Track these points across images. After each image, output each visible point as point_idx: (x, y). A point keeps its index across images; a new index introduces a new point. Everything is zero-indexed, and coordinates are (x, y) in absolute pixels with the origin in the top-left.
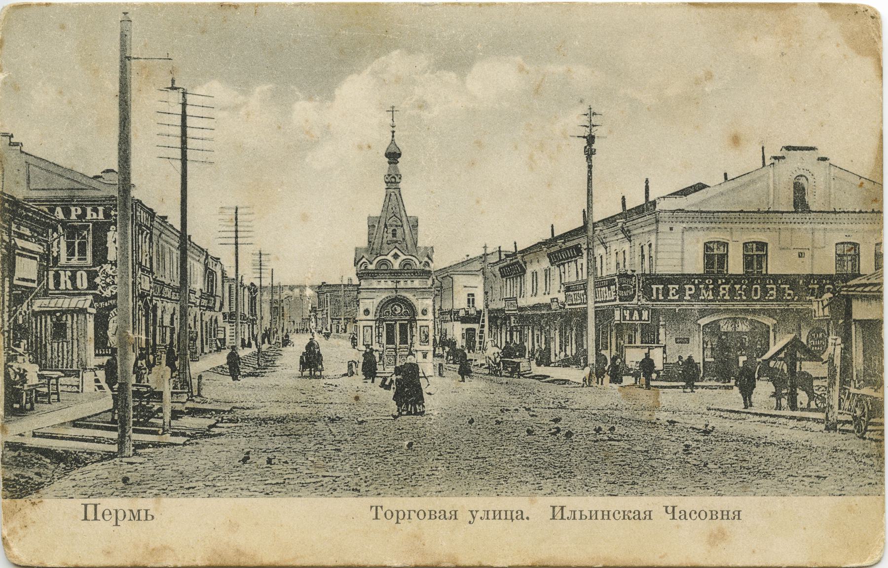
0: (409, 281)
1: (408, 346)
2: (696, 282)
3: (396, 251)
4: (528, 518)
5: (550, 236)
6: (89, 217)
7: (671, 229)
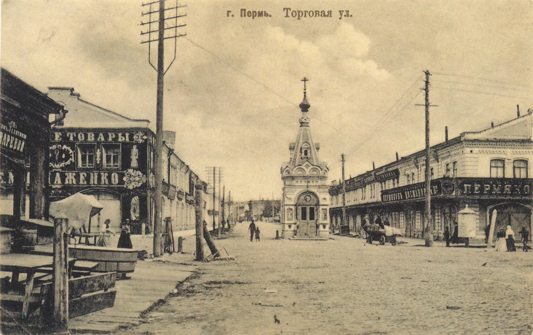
0: (315, 181)
1: (315, 221)
2: (491, 182)
3: (307, 163)
4: (233, 16)
5: (444, 140)
6: (120, 140)
7: (471, 151)
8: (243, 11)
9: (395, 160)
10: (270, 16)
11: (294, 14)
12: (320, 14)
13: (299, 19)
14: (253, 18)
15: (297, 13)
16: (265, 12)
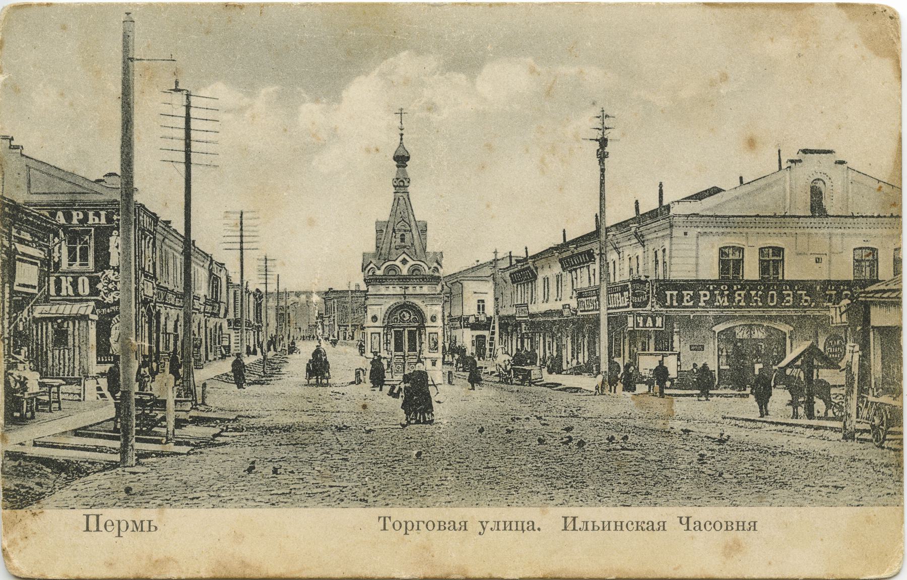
0: (418, 287)
1: (417, 353)
2: (711, 288)
3: (404, 256)
6: (90, 222)
7: (686, 234)
9: (561, 241)
11: (397, 526)
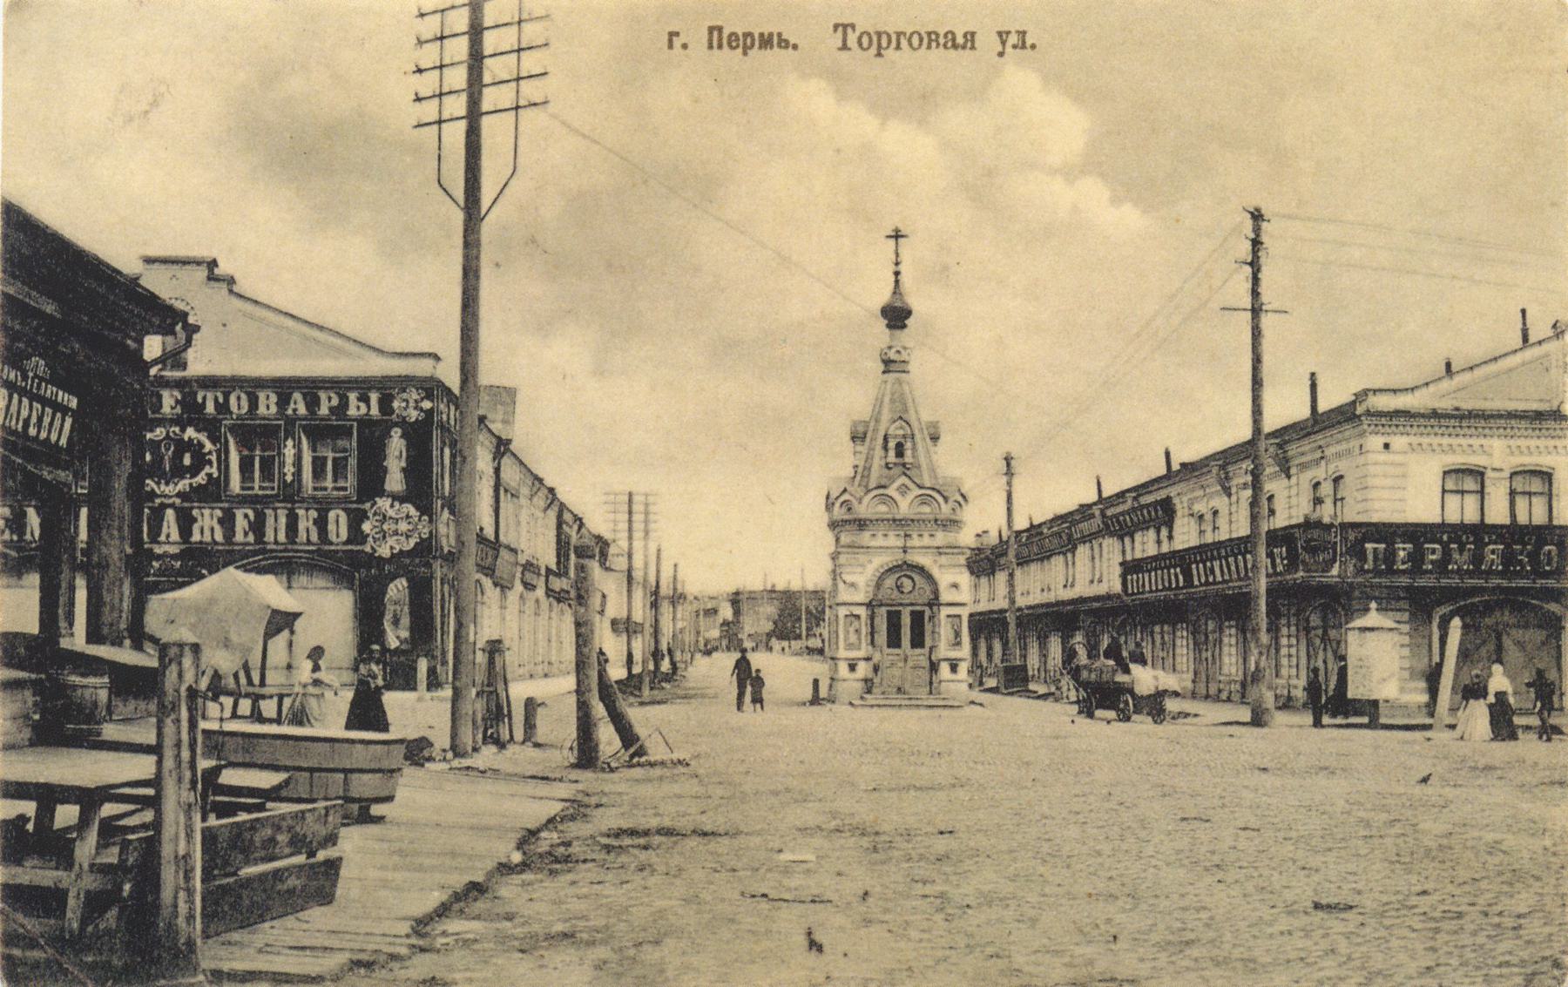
0: (926, 535)
1: (926, 651)
2: (1445, 538)
3: (904, 480)
4: (685, 46)
5: (1305, 413)
6: (352, 412)
7: (1387, 446)
8: (715, 34)
9: (1163, 471)
10: (795, 47)
11: (865, 40)
12: (942, 41)
13: (879, 55)
14: (745, 53)
15: (875, 39)
16: (779, 35)
